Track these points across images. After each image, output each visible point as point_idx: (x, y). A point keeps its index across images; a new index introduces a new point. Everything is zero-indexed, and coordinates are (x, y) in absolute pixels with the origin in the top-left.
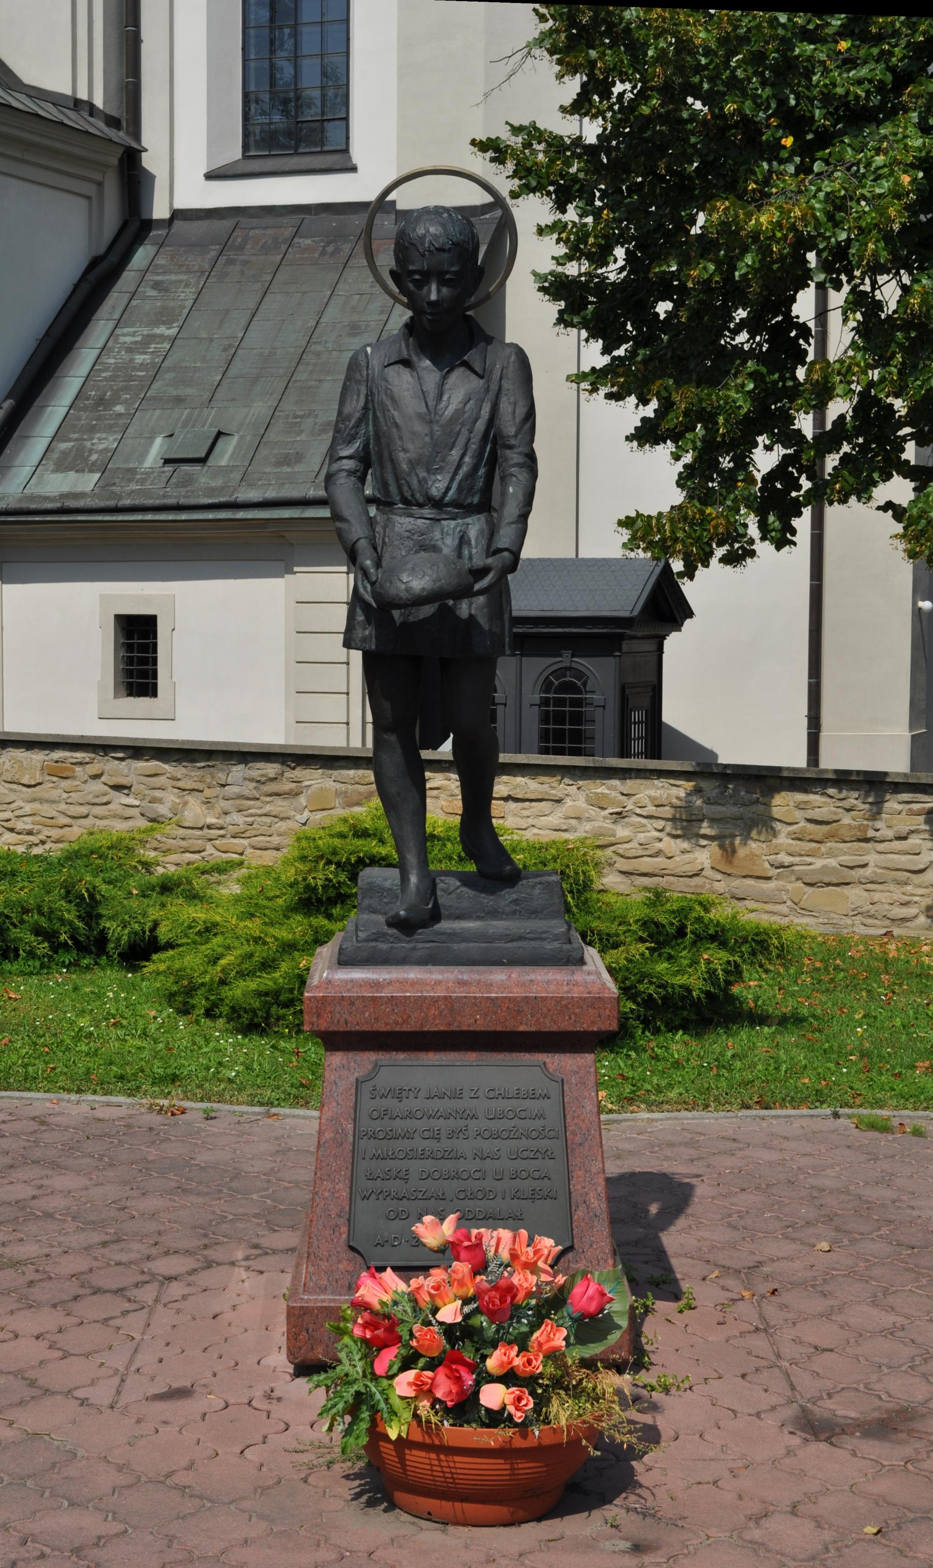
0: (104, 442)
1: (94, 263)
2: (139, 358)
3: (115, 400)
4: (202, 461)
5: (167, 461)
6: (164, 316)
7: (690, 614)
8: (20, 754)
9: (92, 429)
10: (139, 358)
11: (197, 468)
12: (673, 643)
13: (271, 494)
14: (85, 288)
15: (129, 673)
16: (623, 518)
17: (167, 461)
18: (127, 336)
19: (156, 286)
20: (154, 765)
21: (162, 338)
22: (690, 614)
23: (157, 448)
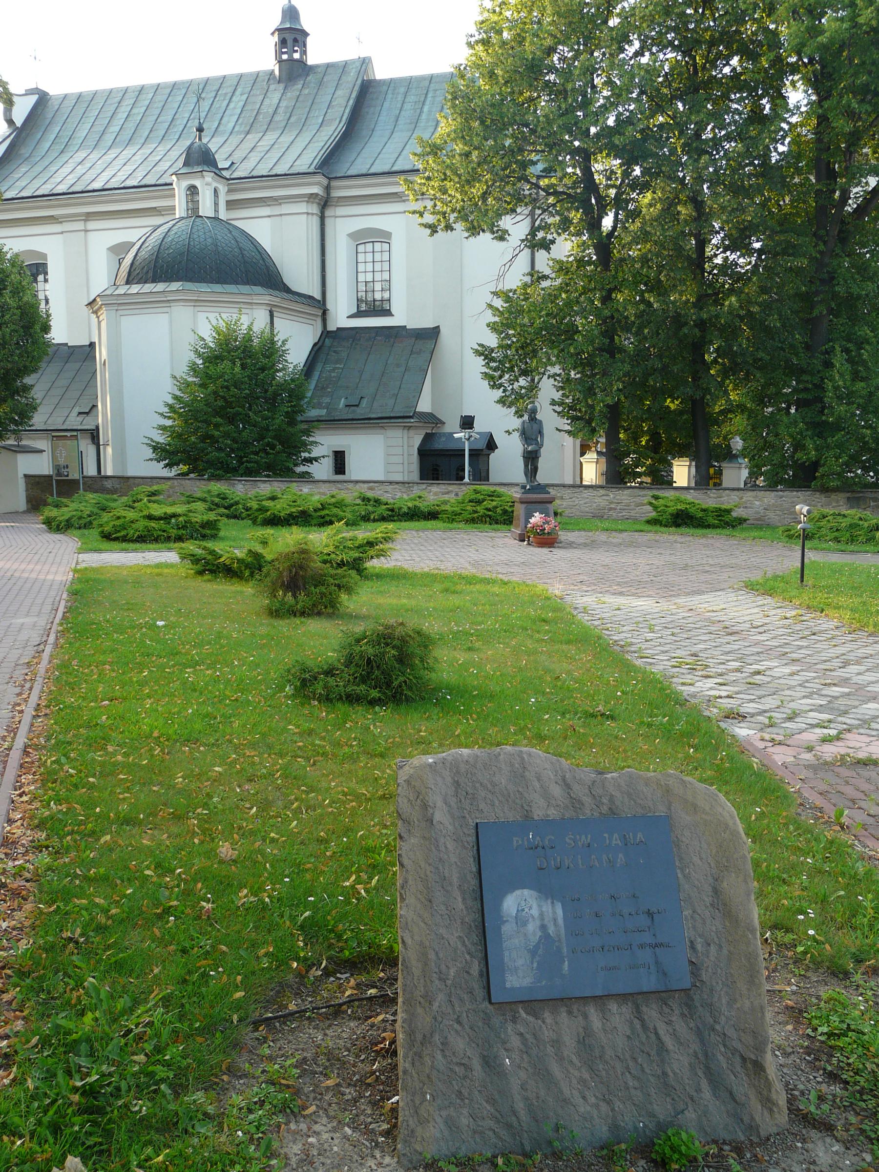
0: (326, 400)
1: (315, 345)
2: (333, 374)
3: (327, 387)
4: (357, 406)
5: (347, 406)
6: (338, 361)
7: (497, 448)
8: (362, 485)
9: (322, 396)
10: (333, 374)
11: (355, 408)
12: (492, 456)
13: (380, 415)
14: (313, 353)
15: (336, 468)
16: (306, 23)
17: (347, 406)
18: (328, 367)
19: (335, 352)
20: (396, 486)
21: (339, 368)
22: (497, 448)
23: (343, 401)
